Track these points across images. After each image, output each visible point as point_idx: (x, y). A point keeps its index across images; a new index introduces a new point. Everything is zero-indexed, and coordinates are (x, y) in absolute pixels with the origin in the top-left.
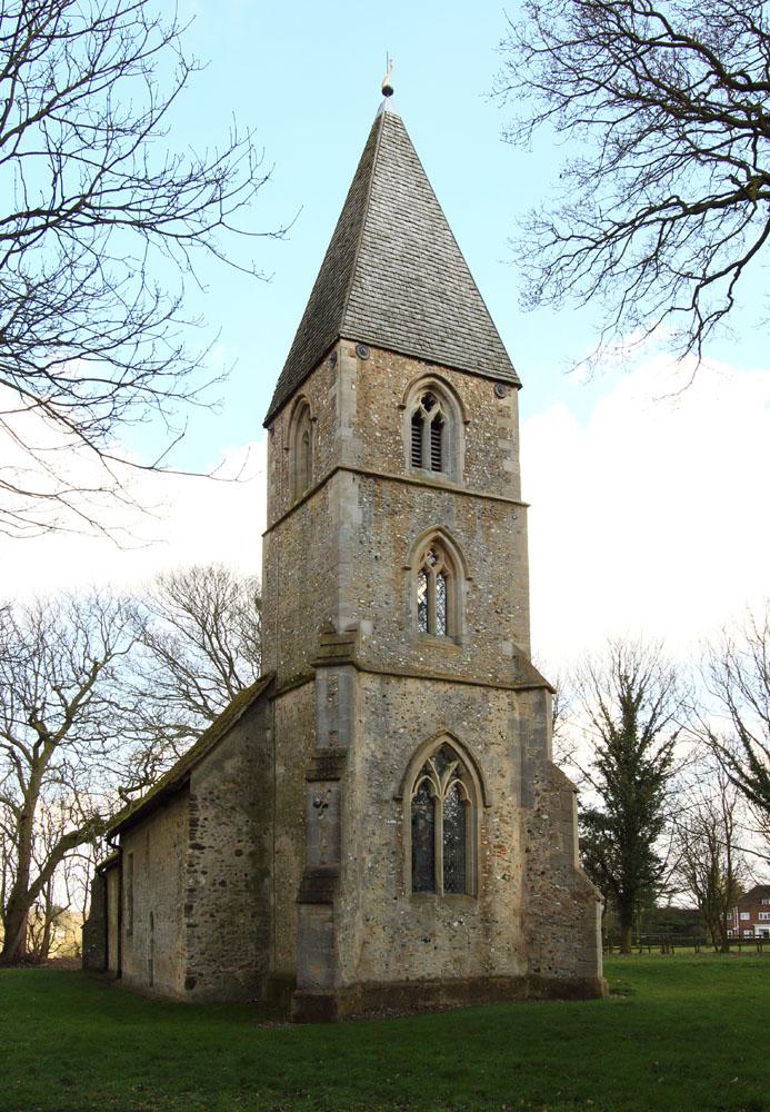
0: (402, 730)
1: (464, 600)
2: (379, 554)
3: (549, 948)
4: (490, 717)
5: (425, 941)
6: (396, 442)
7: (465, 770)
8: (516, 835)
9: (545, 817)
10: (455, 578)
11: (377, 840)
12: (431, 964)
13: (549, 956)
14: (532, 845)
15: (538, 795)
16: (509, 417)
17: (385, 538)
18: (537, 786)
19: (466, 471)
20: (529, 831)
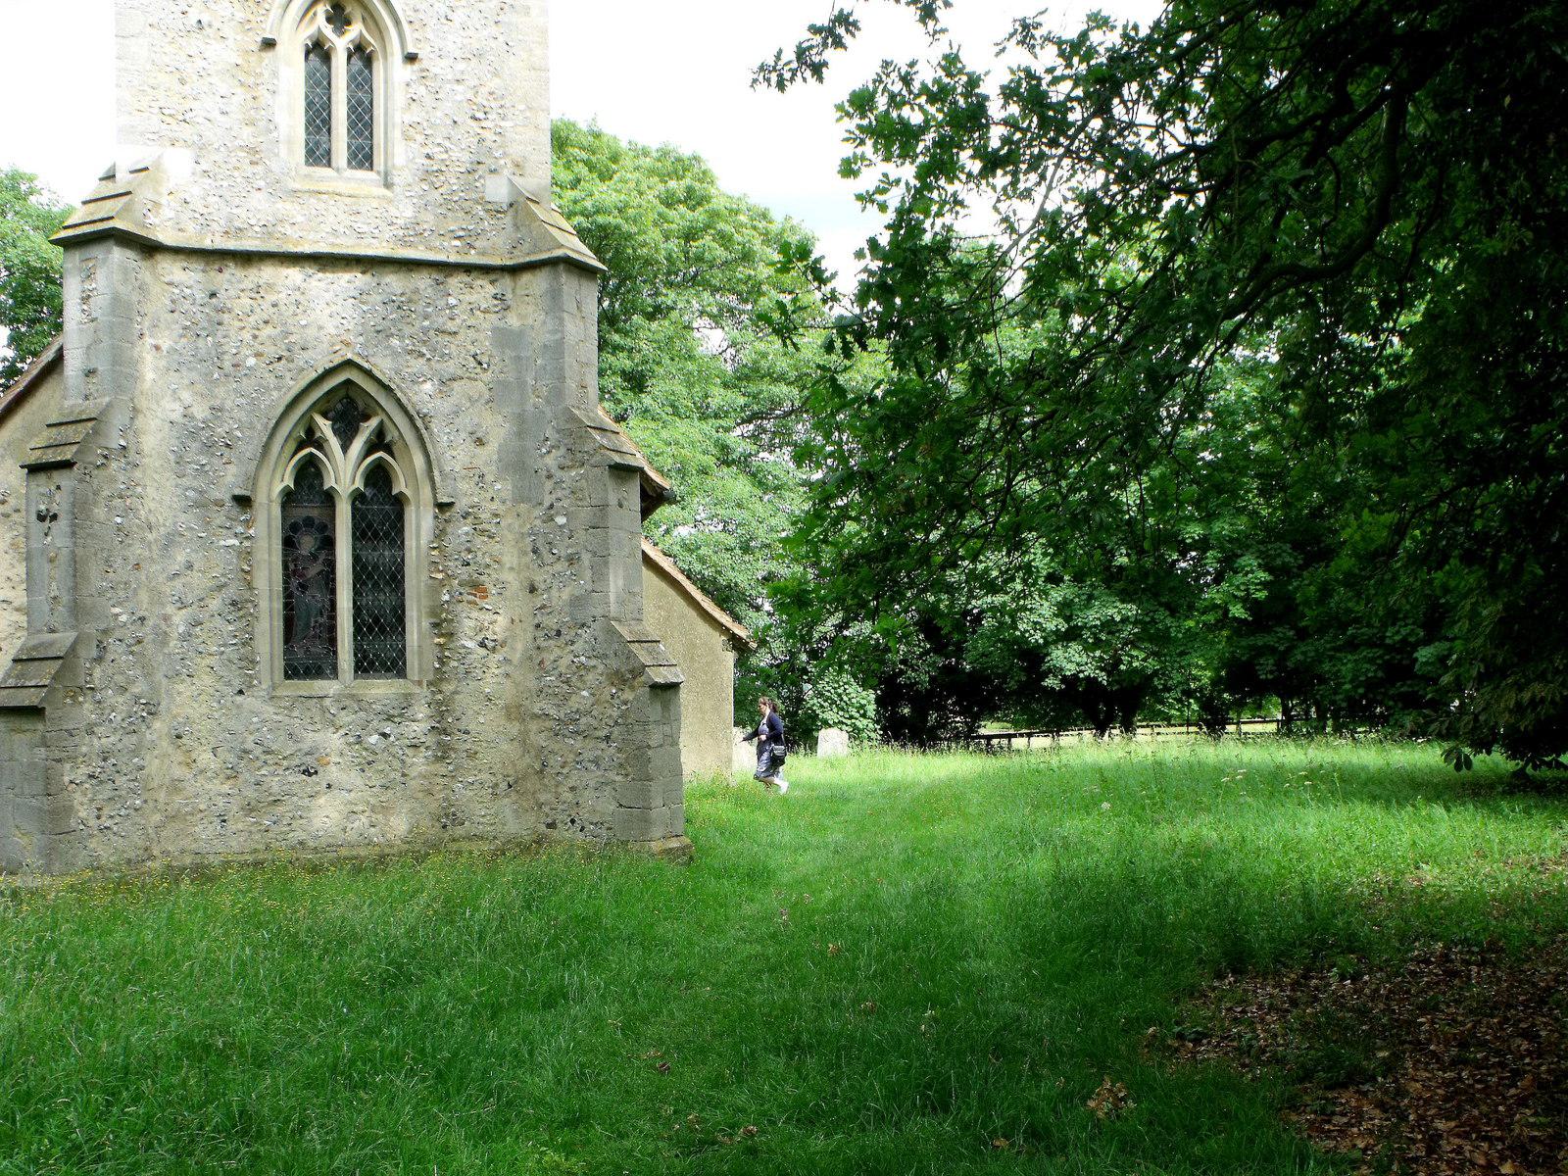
0: (251, 361)
7: (396, 434)
8: (510, 558)
9: (561, 520)
10: (385, 58)
11: (198, 581)
13: (568, 796)
14: (539, 578)
15: (549, 477)
20: (535, 551)
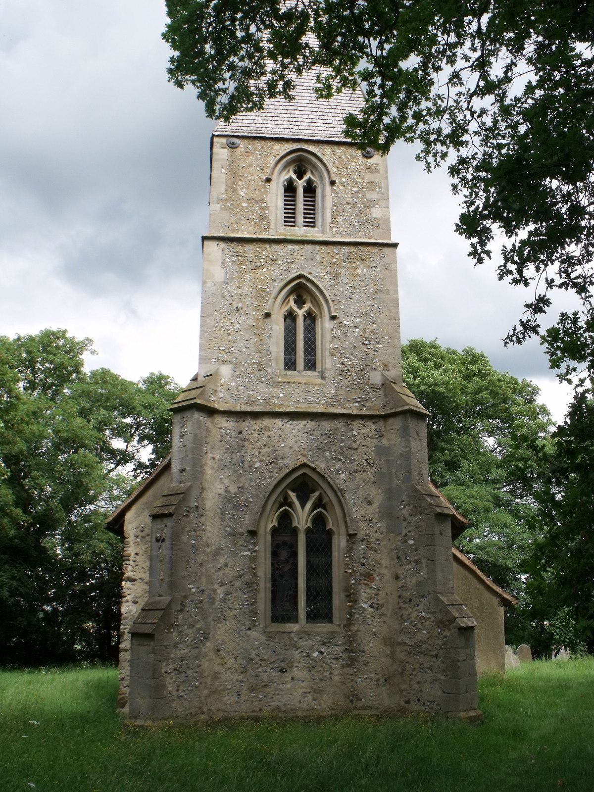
0: (258, 464)
1: (328, 337)
2: (240, 305)
3: (418, 679)
4: (354, 445)
5: (282, 671)
6: (262, 209)
8: (385, 561)
9: (411, 542)
12: (295, 692)
14: (401, 572)
15: (405, 520)
16: (377, 171)
17: (246, 290)
18: (404, 512)
19: (332, 222)
20: (398, 558)
